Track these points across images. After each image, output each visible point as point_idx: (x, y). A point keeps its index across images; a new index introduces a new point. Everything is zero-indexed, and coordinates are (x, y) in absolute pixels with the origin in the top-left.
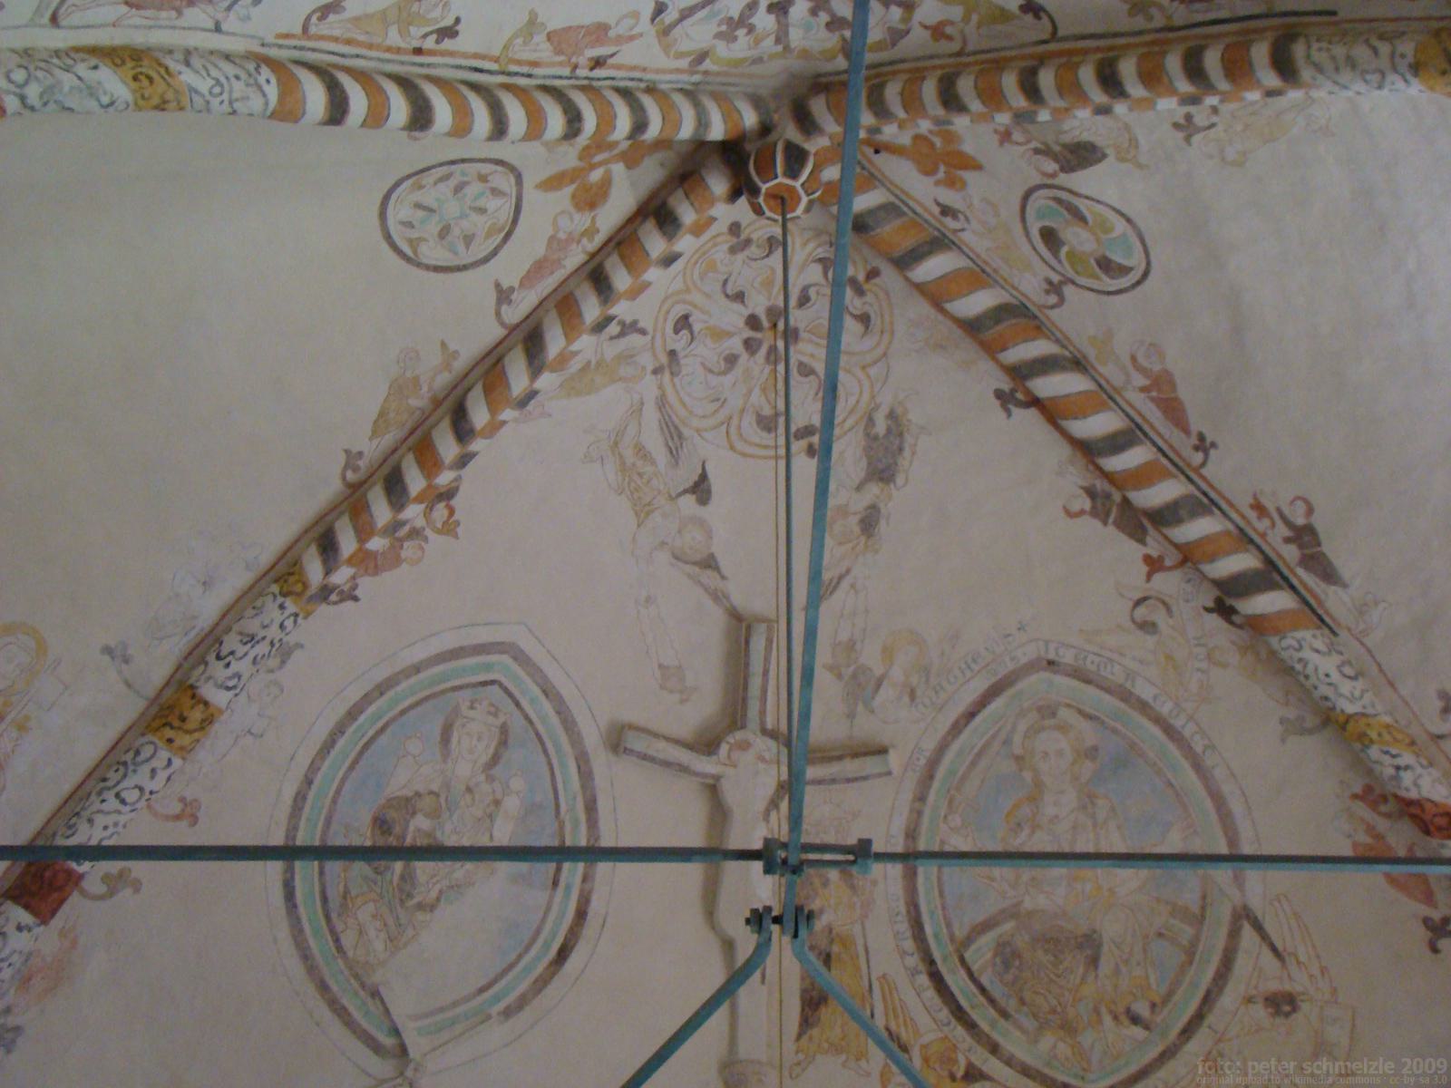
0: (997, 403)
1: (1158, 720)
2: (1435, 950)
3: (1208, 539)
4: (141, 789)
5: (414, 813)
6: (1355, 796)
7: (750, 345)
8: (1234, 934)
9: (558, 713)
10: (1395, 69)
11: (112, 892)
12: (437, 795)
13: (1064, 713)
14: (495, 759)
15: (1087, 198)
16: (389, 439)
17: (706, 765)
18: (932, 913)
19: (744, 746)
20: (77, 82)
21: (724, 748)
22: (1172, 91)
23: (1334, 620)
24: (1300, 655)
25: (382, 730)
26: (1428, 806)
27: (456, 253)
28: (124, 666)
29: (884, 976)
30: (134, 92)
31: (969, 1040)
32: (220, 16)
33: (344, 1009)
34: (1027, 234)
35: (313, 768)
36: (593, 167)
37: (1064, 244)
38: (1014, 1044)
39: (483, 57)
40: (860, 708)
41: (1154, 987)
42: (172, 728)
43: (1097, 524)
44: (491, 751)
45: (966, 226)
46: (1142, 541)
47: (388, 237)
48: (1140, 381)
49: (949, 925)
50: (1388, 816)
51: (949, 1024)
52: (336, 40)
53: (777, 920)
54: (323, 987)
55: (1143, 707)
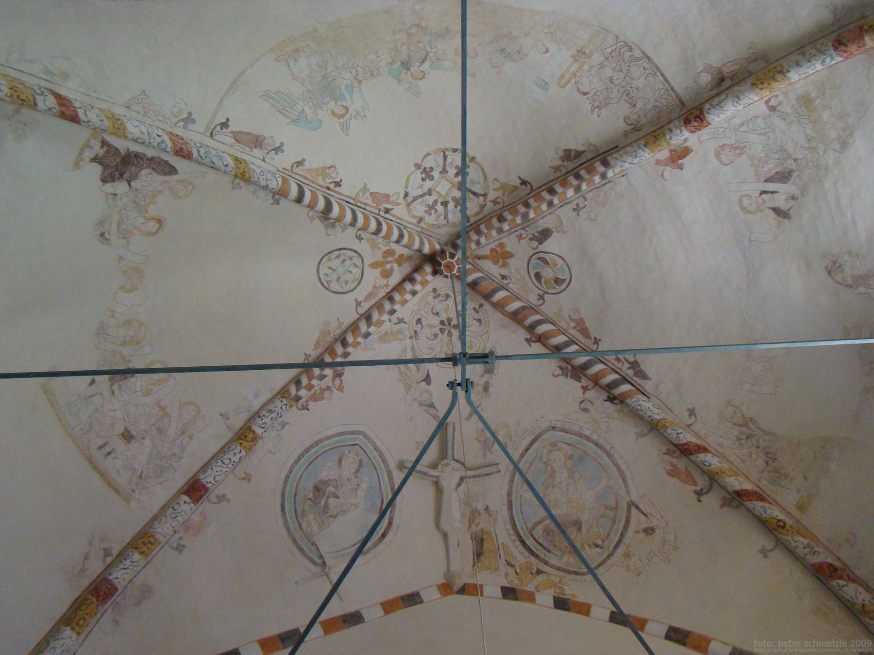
0: (526, 342)
1: (593, 442)
2: (700, 501)
3: (601, 371)
4: (230, 459)
5: (328, 486)
6: (664, 454)
7: (442, 330)
8: (629, 511)
9: (380, 456)
10: (639, 148)
11: (219, 502)
12: (337, 481)
13: (560, 444)
14: (358, 471)
15: (549, 253)
16: (320, 351)
17: (434, 473)
18: (519, 521)
19: (447, 465)
20: (216, 154)
21: (440, 466)
22: (571, 185)
23: (648, 393)
24: (639, 403)
25: (317, 457)
26: (689, 444)
27: (342, 287)
28: (227, 421)
29: (503, 544)
30: (235, 164)
31: (536, 561)
32: (264, 155)
33: (302, 549)
34: (530, 277)
35: (292, 467)
36: (387, 263)
37: (542, 277)
38: (554, 561)
39: (350, 198)
40: (488, 452)
41: (602, 533)
42: (242, 439)
43: (564, 378)
44: (356, 468)
45: (510, 281)
46: (580, 381)
47: (320, 280)
48: (573, 324)
49: (525, 524)
50: (677, 457)
51: (528, 557)
52: (301, 176)
53: (459, 384)
54: (295, 541)
55: (588, 438)
